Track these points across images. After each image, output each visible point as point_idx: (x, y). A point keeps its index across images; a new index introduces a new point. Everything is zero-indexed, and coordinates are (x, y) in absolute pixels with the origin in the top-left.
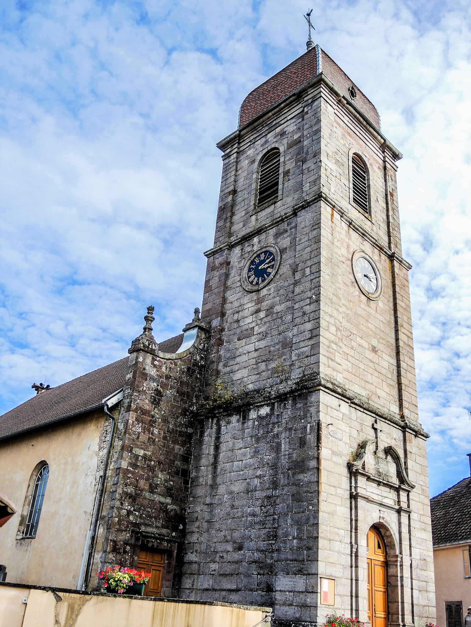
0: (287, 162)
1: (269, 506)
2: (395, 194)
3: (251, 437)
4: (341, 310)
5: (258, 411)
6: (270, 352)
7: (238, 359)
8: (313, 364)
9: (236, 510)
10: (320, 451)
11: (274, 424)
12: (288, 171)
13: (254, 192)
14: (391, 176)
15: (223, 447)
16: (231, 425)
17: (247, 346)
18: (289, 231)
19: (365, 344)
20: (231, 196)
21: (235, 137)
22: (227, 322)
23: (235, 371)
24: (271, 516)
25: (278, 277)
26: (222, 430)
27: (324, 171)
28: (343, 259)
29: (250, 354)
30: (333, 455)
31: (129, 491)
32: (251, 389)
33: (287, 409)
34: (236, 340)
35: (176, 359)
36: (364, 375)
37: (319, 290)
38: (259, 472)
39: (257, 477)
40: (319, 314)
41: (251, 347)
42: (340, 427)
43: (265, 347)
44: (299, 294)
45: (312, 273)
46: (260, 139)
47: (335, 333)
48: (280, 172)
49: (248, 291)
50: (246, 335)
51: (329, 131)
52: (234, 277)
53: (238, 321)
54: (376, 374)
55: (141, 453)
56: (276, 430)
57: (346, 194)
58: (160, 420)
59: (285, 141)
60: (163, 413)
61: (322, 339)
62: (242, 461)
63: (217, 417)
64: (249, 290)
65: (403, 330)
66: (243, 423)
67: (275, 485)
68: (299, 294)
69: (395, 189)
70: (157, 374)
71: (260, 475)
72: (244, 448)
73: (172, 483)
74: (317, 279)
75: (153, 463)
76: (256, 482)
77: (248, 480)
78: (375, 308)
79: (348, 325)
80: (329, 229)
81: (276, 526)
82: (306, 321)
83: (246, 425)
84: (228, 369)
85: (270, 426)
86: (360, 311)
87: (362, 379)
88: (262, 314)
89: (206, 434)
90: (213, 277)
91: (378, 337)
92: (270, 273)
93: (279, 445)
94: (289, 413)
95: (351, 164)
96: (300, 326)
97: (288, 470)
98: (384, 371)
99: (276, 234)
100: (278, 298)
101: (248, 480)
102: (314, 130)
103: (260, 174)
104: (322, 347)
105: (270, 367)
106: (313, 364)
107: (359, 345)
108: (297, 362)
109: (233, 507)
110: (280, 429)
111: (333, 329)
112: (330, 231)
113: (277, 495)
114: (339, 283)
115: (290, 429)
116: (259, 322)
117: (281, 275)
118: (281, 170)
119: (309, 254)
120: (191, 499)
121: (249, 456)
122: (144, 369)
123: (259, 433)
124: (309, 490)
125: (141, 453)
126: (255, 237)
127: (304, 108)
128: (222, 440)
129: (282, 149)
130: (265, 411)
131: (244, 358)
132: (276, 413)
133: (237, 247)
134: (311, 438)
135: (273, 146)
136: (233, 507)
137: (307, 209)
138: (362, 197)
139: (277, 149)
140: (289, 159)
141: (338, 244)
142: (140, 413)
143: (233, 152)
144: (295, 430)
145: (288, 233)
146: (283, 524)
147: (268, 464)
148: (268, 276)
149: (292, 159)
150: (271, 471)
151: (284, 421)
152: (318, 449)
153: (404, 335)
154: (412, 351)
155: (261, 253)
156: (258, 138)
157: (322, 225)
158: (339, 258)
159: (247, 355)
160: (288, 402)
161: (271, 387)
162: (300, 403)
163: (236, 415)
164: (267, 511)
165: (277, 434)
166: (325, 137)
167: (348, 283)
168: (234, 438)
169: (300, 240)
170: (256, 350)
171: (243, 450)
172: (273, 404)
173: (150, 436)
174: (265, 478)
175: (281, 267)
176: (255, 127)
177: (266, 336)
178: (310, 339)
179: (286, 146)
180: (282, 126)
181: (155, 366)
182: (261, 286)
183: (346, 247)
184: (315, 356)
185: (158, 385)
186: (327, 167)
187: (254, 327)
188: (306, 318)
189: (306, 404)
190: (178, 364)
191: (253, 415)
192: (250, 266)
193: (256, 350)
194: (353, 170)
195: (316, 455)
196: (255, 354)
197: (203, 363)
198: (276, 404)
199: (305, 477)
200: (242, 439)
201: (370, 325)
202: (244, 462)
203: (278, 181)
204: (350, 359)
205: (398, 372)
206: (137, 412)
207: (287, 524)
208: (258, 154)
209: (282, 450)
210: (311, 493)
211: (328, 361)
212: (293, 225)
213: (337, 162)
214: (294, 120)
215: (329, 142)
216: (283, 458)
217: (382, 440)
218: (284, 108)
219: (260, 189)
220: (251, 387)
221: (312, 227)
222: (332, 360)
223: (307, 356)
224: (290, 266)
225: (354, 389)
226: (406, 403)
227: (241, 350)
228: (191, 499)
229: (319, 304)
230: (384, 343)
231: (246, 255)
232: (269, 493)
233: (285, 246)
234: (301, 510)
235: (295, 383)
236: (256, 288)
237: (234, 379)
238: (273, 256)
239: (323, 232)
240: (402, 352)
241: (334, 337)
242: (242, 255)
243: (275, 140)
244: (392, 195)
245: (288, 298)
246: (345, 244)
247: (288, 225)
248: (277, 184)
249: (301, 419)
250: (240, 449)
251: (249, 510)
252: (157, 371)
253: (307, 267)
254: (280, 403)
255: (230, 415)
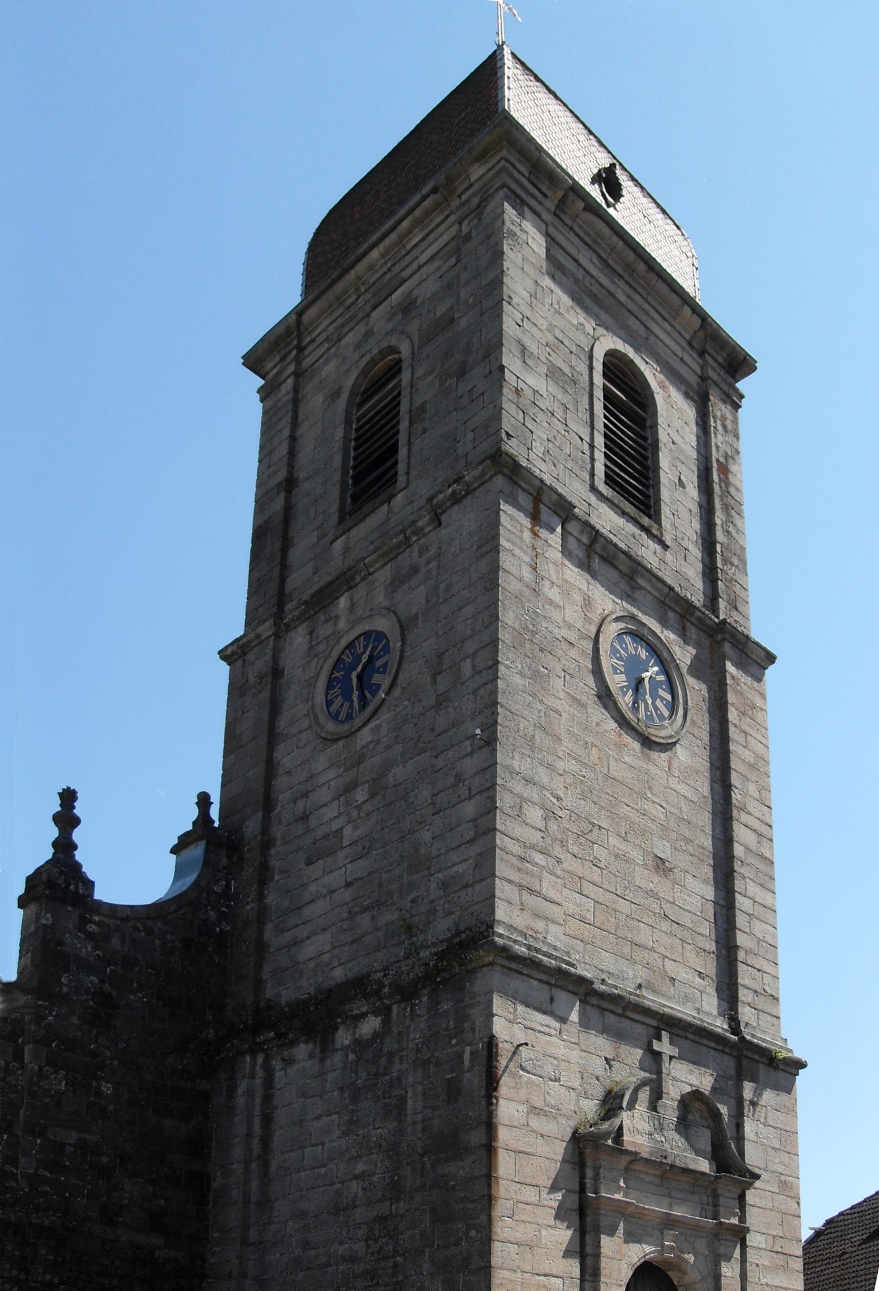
0: (418, 386)
1: (384, 1237)
2: (733, 468)
3: (341, 1089)
4: (560, 765)
5: (356, 1027)
6: (380, 885)
7: (307, 912)
8: (478, 903)
9: (313, 1253)
10: (494, 1108)
11: (390, 1054)
12: (422, 408)
13: (337, 477)
14: (723, 418)
15: (281, 1118)
16: (296, 1067)
17: (327, 877)
18: (423, 570)
19: (635, 854)
20: (282, 495)
21: (288, 332)
22: (280, 822)
23: (302, 941)
24: (389, 1258)
25: (396, 693)
26: (277, 1080)
27: (512, 396)
28: (573, 637)
29: (334, 895)
30: (531, 1115)
31: (13, 1219)
32: (339, 980)
33: (419, 1016)
34: (303, 865)
35: (149, 919)
36: (630, 929)
37: (495, 714)
38: (360, 1167)
39: (356, 1177)
40: (494, 776)
41: (336, 879)
42: (551, 1050)
43: (370, 873)
44: (445, 731)
45: (476, 672)
46: (351, 329)
47: (541, 824)
48: (402, 413)
49: (329, 740)
50: (324, 849)
51: (530, 284)
52: (294, 710)
53: (305, 817)
54: (665, 926)
55: (73, 1137)
56: (397, 1067)
57: (583, 462)
58: (116, 1062)
59: (414, 328)
60: (122, 1045)
61: (499, 839)
62: (323, 1144)
63: (263, 1050)
64: (329, 737)
65: (744, 817)
66: (322, 1060)
67: (395, 1191)
68: (445, 731)
69: (733, 455)
70: (98, 955)
71: (364, 1172)
72: (327, 1116)
73: (162, 1202)
74: (489, 687)
75: (105, 1159)
76: (355, 1187)
77: (337, 1186)
78: (666, 764)
79: (584, 807)
80: (525, 552)
81: (400, 1278)
82: (463, 797)
83: (328, 1063)
84: (287, 936)
85: (383, 1061)
86: (616, 771)
87: (625, 939)
88: (361, 795)
89: (240, 1091)
90: (243, 713)
91: (674, 836)
92: (379, 686)
93: (403, 1100)
94: (422, 1025)
95: (599, 380)
96: (448, 812)
97: (422, 1156)
98: (686, 920)
99: (392, 582)
100: (399, 748)
101: (337, 1186)
102: (484, 283)
103: (354, 427)
104: (502, 859)
105: (381, 922)
106: (478, 903)
107: (617, 856)
108: (442, 902)
109: (306, 1245)
110: (405, 1066)
111: (534, 815)
112: (527, 559)
113: (402, 1212)
114: (556, 697)
115: (425, 1063)
116: (355, 814)
117: (403, 689)
118: (404, 407)
119: (469, 622)
120: (216, 1235)
121: (337, 1133)
122: (60, 943)
123: (357, 1079)
124: (468, 1195)
125: (73, 1137)
126: (342, 595)
127: (460, 224)
128: (277, 1101)
129: (405, 349)
130: (370, 1025)
131: (321, 906)
132: (395, 1030)
133: (300, 629)
134: (473, 1079)
135: (384, 344)
136: (306, 1245)
137: (464, 502)
138: (633, 474)
139: (392, 350)
140: (426, 374)
141: (553, 594)
142: (57, 1046)
143: (286, 374)
144: (437, 1065)
145: (420, 576)
146: (413, 1273)
147: (380, 1146)
148: (374, 693)
149: (432, 372)
150: (387, 1163)
151: (411, 1045)
152: (490, 1103)
153: (749, 831)
154: (768, 870)
155: (358, 638)
156: (347, 328)
157: (503, 541)
158: (556, 631)
159: (328, 898)
160: (420, 1001)
161: (385, 969)
162: (448, 1000)
163: (306, 1042)
164: (381, 1248)
165: (399, 1079)
166: (515, 300)
167: (583, 698)
168: (303, 1095)
169: (449, 587)
170: (348, 885)
171: (325, 1119)
172: (389, 1008)
173: (92, 1099)
174: (375, 1179)
175: (405, 666)
176: (338, 298)
177: (370, 847)
178: (472, 841)
179: (416, 338)
180: (406, 284)
181: (90, 936)
182: (358, 721)
183: (581, 602)
184: (484, 884)
185: (102, 982)
186: (521, 385)
187: (341, 829)
188: (463, 791)
189: (462, 1001)
190: (156, 930)
191: (343, 1037)
192: (332, 673)
193: (348, 885)
194: (606, 397)
195: (484, 1118)
196: (347, 895)
197: (229, 928)
198: (395, 1007)
199: (459, 1169)
200: (321, 1096)
201: (649, 807)
202: (326, 1146)
203: (397, 441)
204: (588, 888)
205: (728, 920)
206: (50, 1046)
207: (421, 1273)
208: (349, 370)
209: (409, 1112)
210: (472, 1202)
211: (521, 895)
212: (433, 551)
213: (554, 373)
214: (436, 264)
215: (528, 313)
216: (409, 1129)
217: (675, 1079)
218: (409, 232)
219: (354, 468)
220: (338, 974)
221: (477, 549)
222: (532, 891)
223: (466, 886)
224: (427, 661)
225: (601, 964)
226: (745, 991)
227: (313, 888)
228: (216, 1235)
229: (495, 750)
230: (691, 849)
231: (321, 647)
232: (384, 1209)
233: (414, 612)
234: (452, 1240)
235: (436, 954)
236: (345, 728)
237: (302, 957)
238: (385, 641)
239: (506, 561)
240: (742, 871)
241: (539, 834)
242: (311, 648)
243: (390, 326)
244: (724, 470)
245: (421, 745)
246: (577, 597)
247: (421, 553)
248: (394, 449)
249: (450, 1037)
250: (318, 1118)
251: (341, 1250)
252: (97, 947)
253: (464, 659)
254: (403, 1005)
255: (292, 1044)
